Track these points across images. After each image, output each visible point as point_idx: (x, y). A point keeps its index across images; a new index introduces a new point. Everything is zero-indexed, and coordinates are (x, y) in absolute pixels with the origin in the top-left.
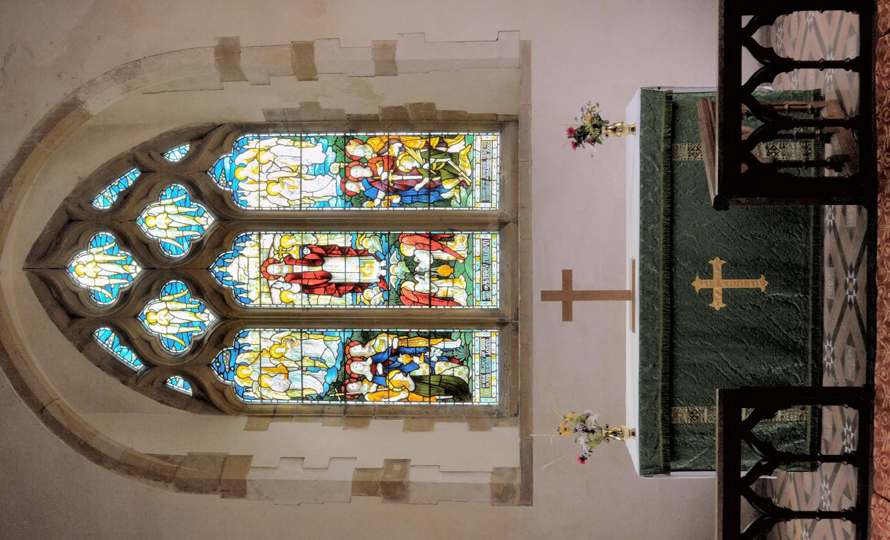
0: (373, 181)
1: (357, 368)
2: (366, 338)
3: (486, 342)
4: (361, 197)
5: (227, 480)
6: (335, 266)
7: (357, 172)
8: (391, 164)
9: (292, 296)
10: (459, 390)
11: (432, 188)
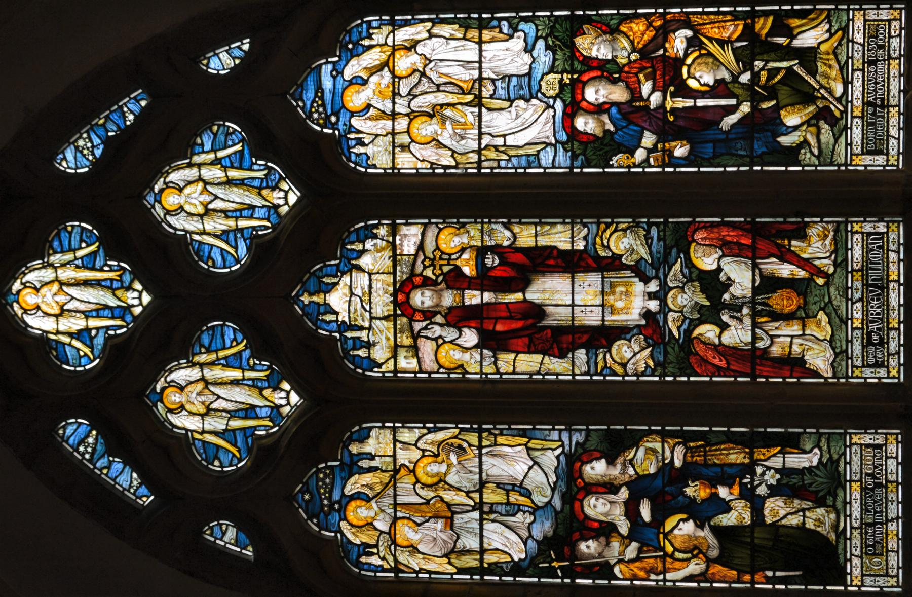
1: (597, 507)
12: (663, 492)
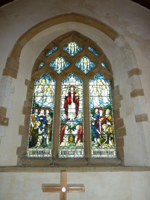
0: (98, 117)
1: (42, 112)
2: (51, 114)
3: (48, 153)
4: (93, 113)
5: (11, 70)
6: (73, 105)
7: (101, 112)
8: (104, 122)
9: (65, 93)
10: (33, 144)
11: (98, 136)
12: (44, 121)
